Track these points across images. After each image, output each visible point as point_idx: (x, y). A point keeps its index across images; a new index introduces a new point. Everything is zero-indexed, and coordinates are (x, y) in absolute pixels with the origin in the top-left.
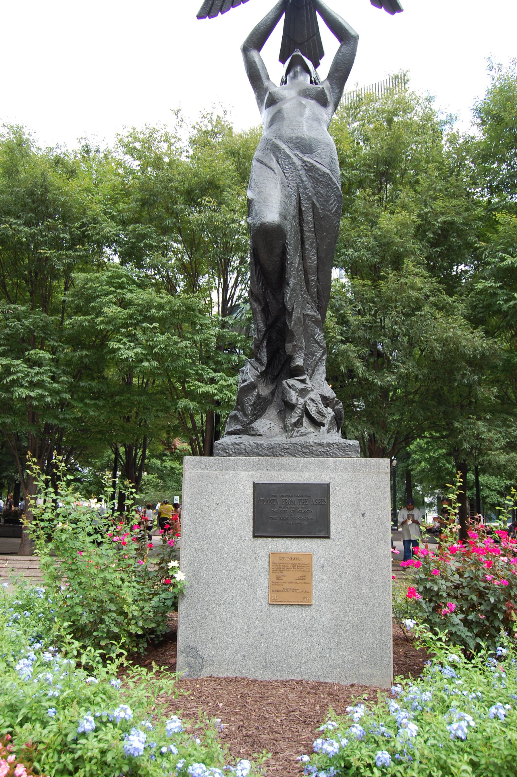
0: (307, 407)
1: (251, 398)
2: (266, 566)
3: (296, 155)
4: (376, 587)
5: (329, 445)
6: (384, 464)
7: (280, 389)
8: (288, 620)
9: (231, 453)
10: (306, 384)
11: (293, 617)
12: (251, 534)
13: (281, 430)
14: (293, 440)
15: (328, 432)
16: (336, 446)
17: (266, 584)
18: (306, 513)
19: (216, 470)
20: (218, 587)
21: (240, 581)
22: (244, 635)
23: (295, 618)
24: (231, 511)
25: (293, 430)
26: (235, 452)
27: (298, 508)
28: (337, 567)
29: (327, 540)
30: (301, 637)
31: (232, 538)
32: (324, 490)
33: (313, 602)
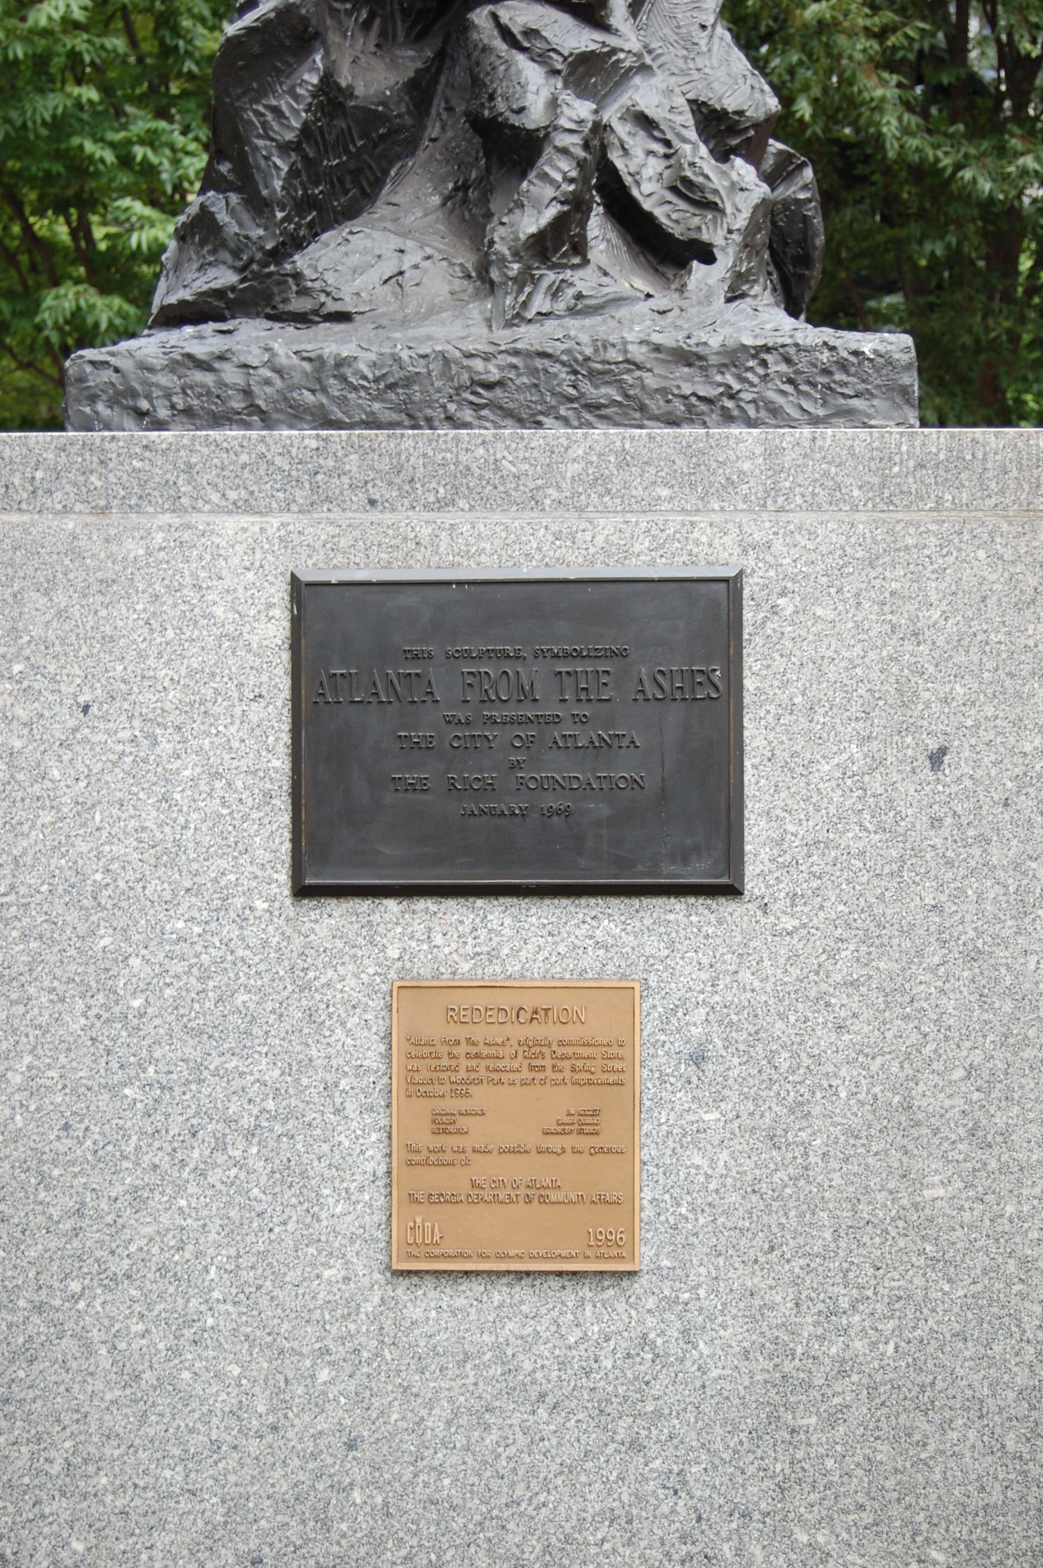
0: (615, 157)
1: (287, 107)
5: (735, 357)
7: (460, 75)
8: (501, 1359)
9: (163, 413)
10: (606, 28)
11: (528, 1344)
12: (283, 876)
13: (458, 284)
14: (529, 336)
15: (734, 296)
16: (777, 366)
17: (373, 1162)
18: (601, 748)
19: (66, 510)
20: (95, 1181)
21: (220, 1145)
22: (253, 1446)
23: (543, 1349)
24: (166, 747)
25: (526, 279)
26: (188, 412)
27: (556, 721)
28: (783, 1061)
29: (725, 907)
30: (577, 1452)
31: (170, 904)
32: (710, 615)
33: (645, 1255)
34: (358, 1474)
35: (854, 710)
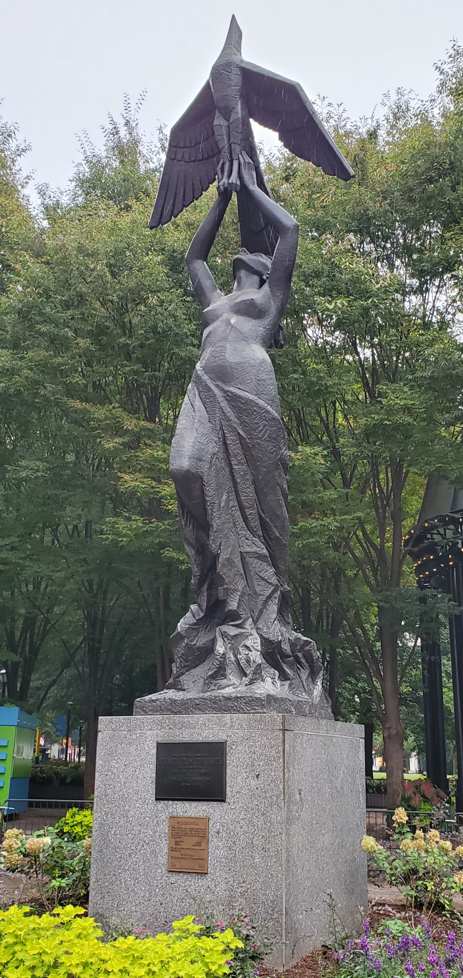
3: (217, 386)
4: (268, 856)
6: (278, 720)
17: (166, 850)
22: (146, 903)
24: (137, 773)
27: (196, 769)
29: (223, 803)
34: (162, 910)
35: (244, 767)
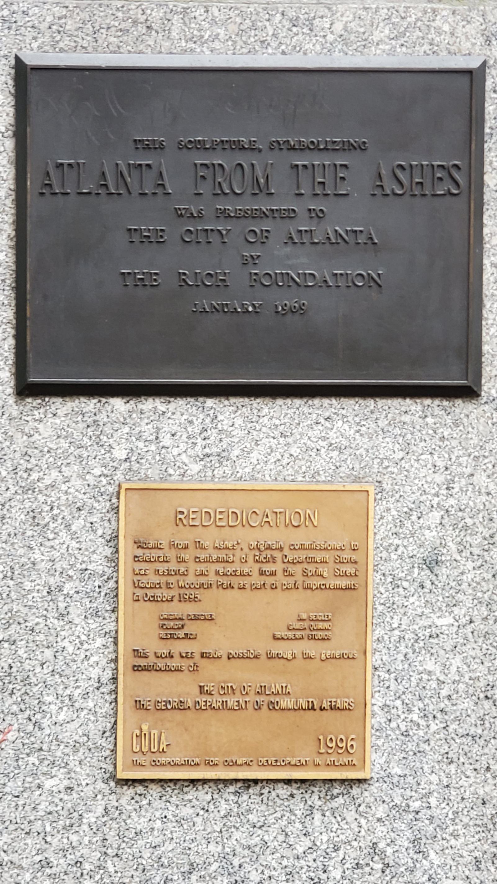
2: (98, 564)
11: (254, 853)
17: (98, 669)
23: (270, 859)
29: (460, 406)
33: (375, 763)
